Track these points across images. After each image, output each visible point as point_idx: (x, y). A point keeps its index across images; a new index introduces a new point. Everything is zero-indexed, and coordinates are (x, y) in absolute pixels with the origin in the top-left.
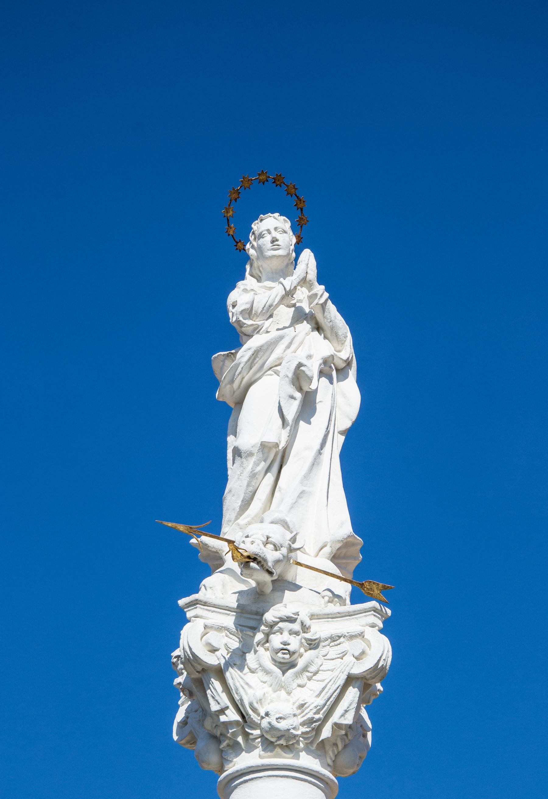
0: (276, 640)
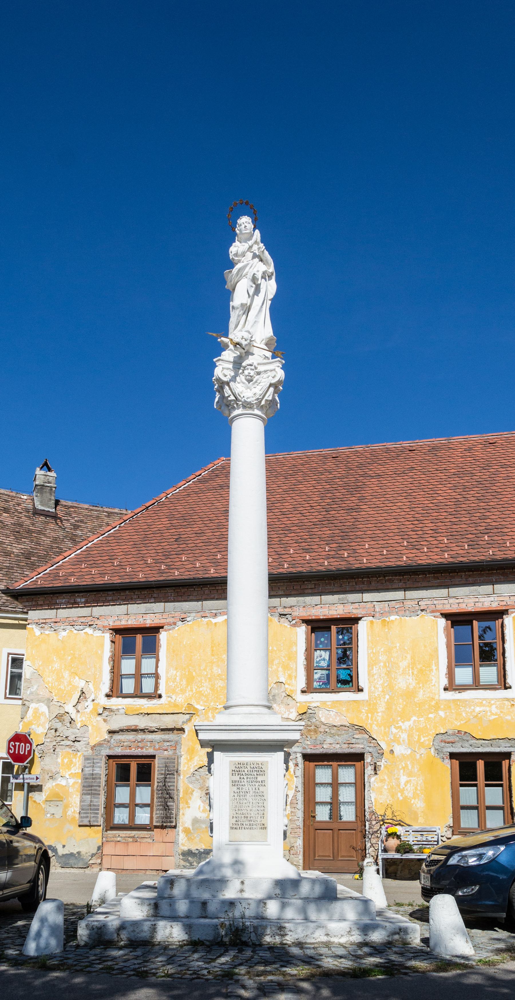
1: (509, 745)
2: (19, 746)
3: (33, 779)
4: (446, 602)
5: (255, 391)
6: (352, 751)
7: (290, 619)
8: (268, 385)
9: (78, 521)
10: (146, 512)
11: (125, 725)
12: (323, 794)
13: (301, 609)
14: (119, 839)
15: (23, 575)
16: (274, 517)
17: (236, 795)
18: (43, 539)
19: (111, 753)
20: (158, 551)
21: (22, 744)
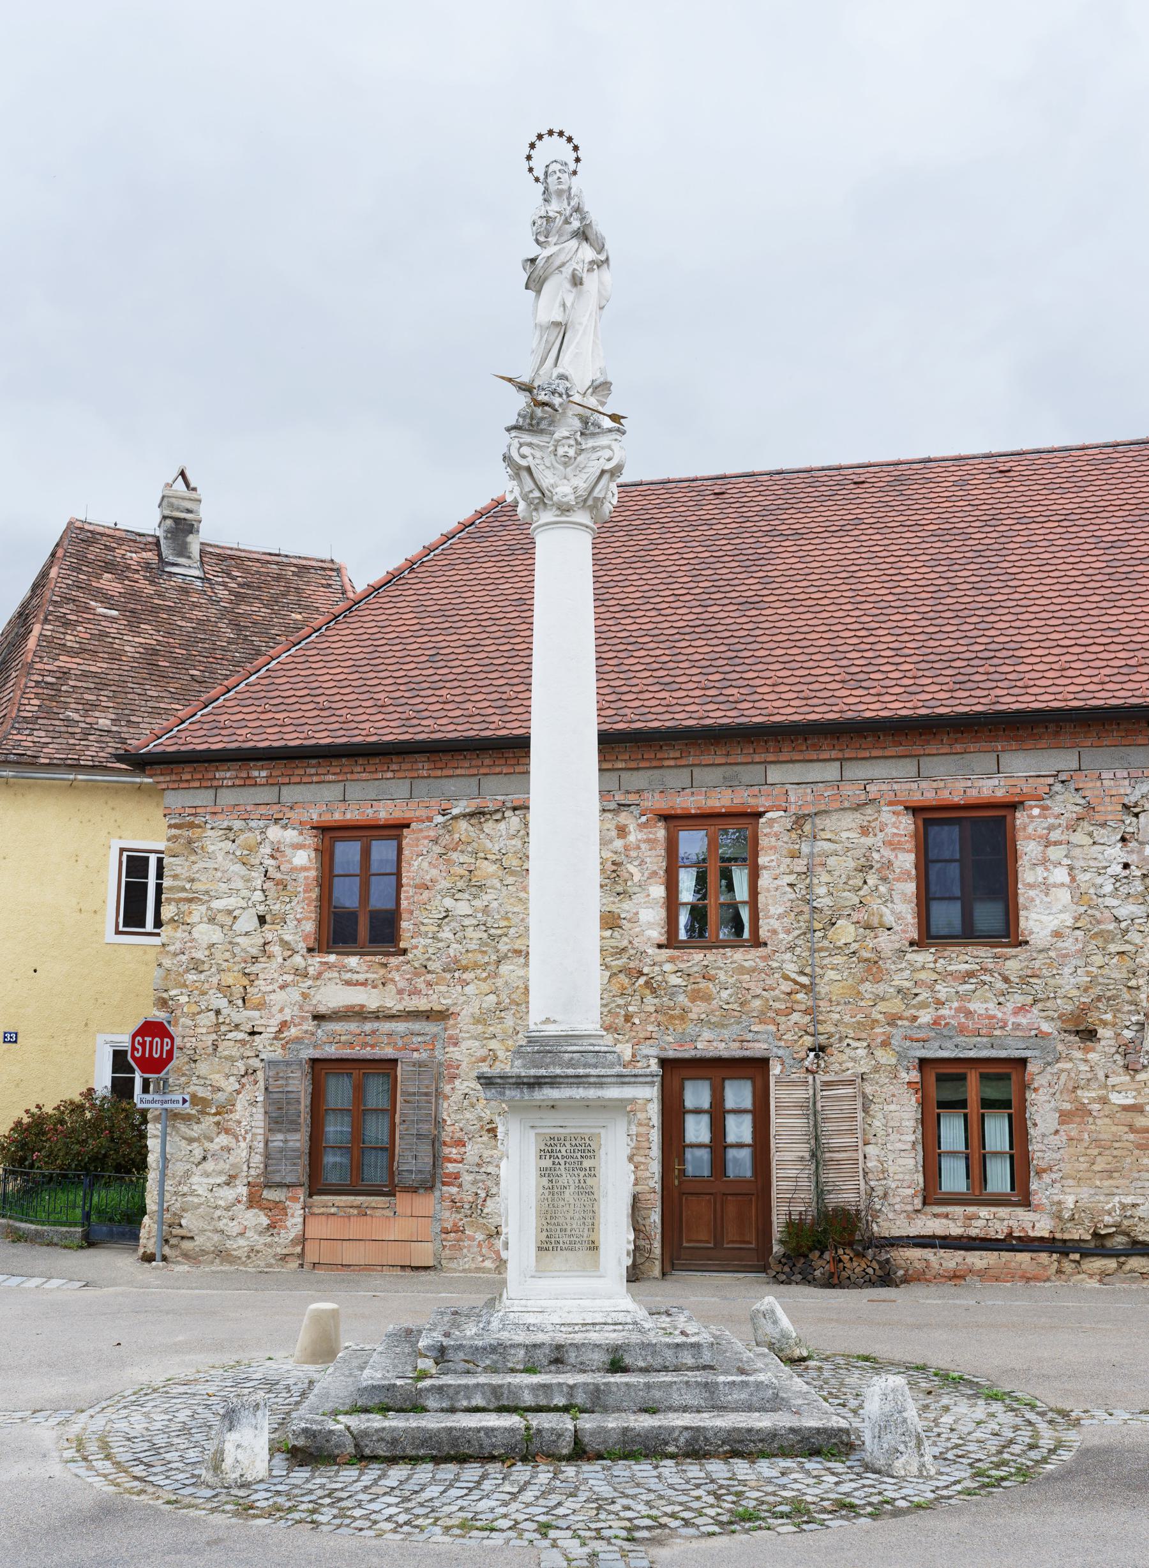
1: (1024, 1046)
2: (151, 1043)
3: (178, 1102)
4: (914, 786)
5: (575, 482)
6: (748, 1054)
7: (637, 813)
8: (598, 474)
9: (240, 585)
10: (376, 600)
11: (341, 1004)
12: (697, 1130)
13: (657, 796)
14: (333, 1210)
15: (145, 698)
16: (608, 615)
17: (546, 1192)
18: (179, 623)
19: (317, 1054)
20: (398, 681)
21: (157, 1039)
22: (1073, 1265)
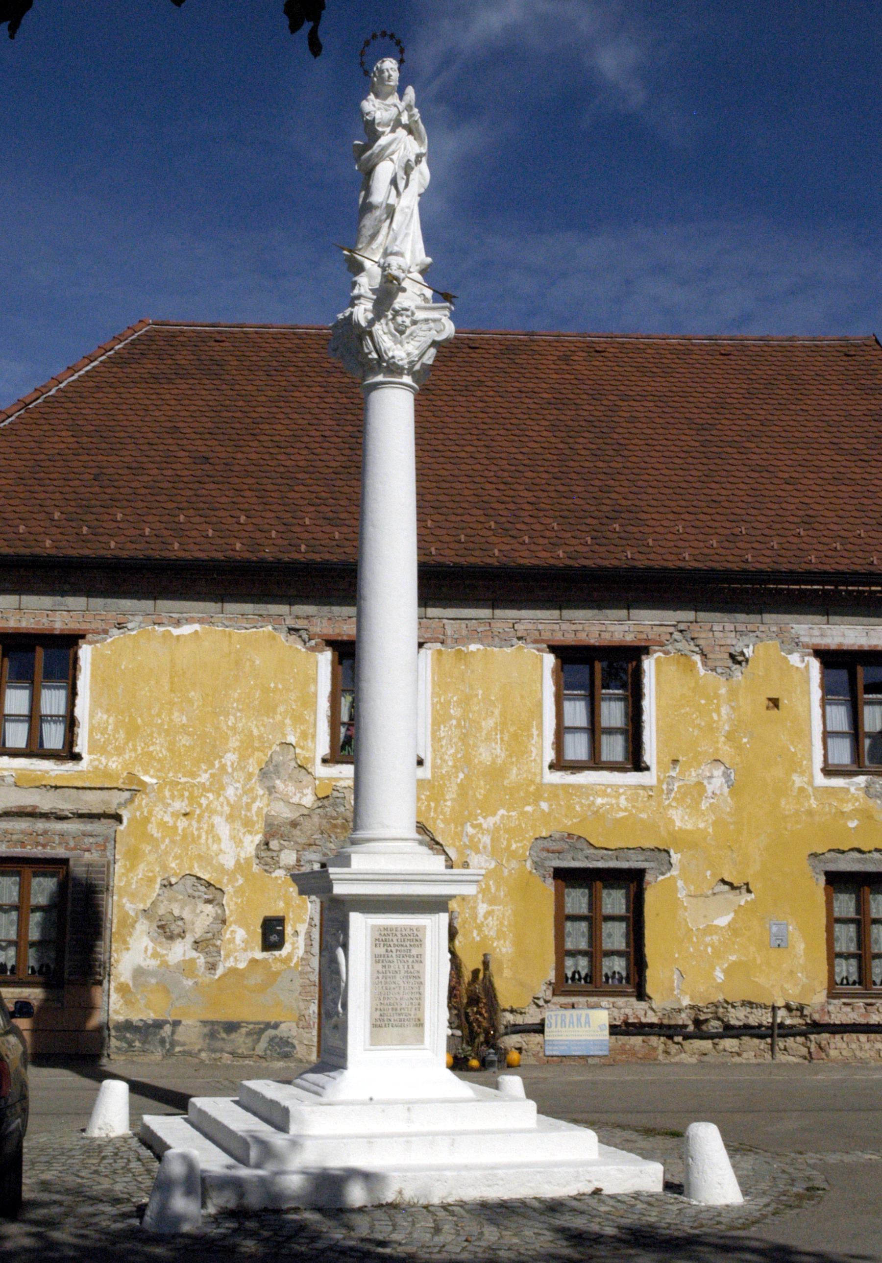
0: (399, 319)
4: (556, 627)
17: (380, 976)
22: (677, 1047)
